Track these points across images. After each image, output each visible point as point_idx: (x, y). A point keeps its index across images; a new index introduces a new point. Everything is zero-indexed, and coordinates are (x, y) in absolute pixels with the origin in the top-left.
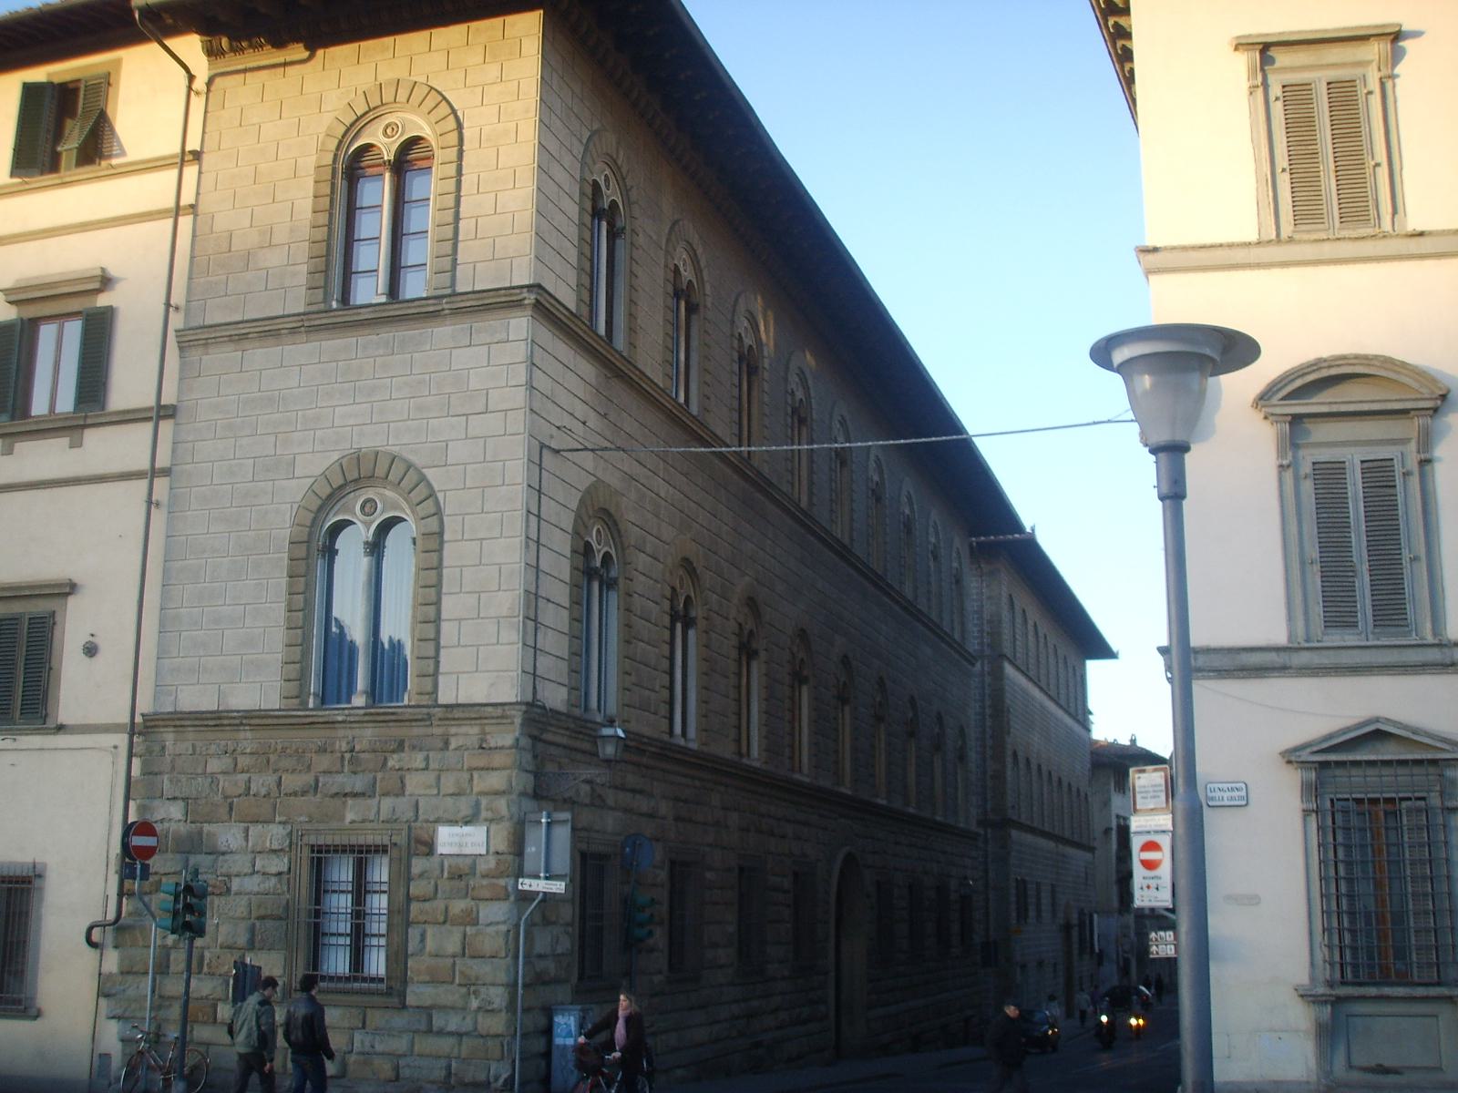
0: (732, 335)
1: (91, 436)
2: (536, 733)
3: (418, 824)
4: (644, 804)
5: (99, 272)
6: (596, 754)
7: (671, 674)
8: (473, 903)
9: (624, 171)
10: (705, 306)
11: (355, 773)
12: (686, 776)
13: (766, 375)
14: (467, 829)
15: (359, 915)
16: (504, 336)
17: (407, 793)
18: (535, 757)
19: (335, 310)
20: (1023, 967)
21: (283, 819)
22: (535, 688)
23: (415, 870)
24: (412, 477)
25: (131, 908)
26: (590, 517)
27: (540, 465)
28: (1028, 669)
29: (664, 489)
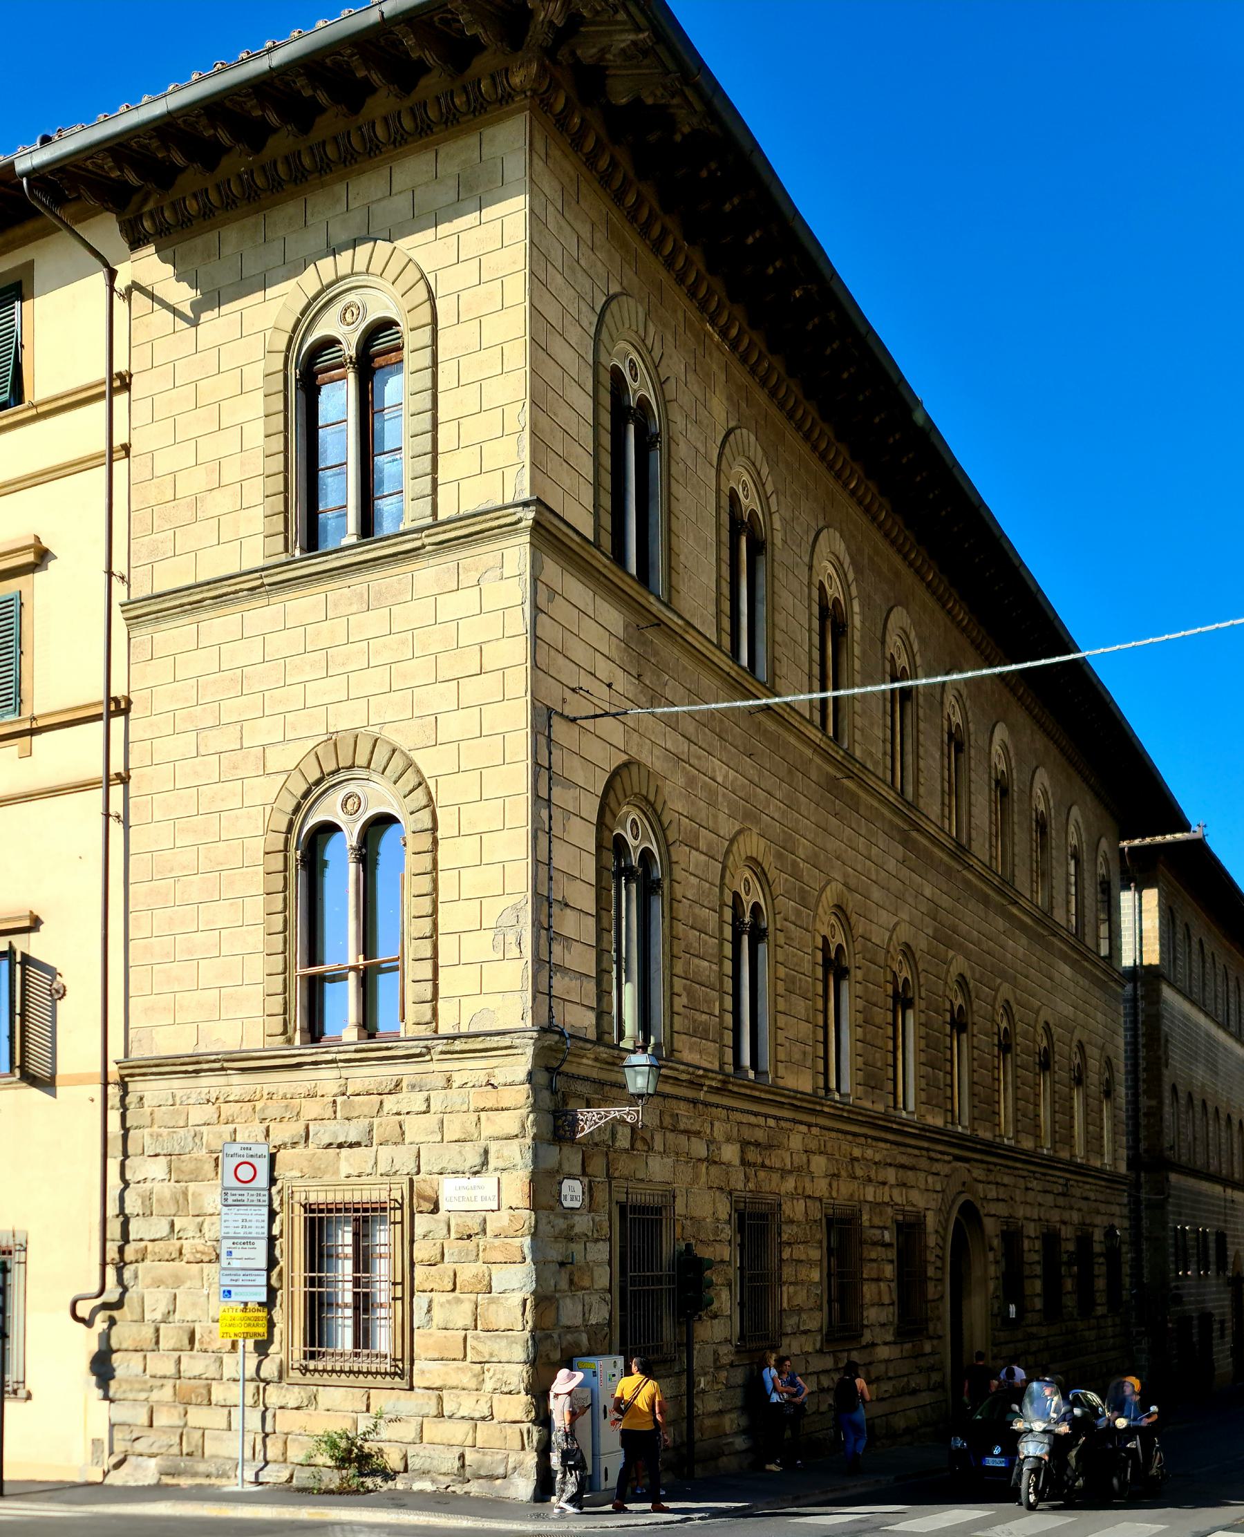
3: (421, 1176)
5: (32, 541)
6: (623, 1086)
12: (756, 1114)
14: (476, 1181)
17: (407, 1141)
28: (1191, 991)
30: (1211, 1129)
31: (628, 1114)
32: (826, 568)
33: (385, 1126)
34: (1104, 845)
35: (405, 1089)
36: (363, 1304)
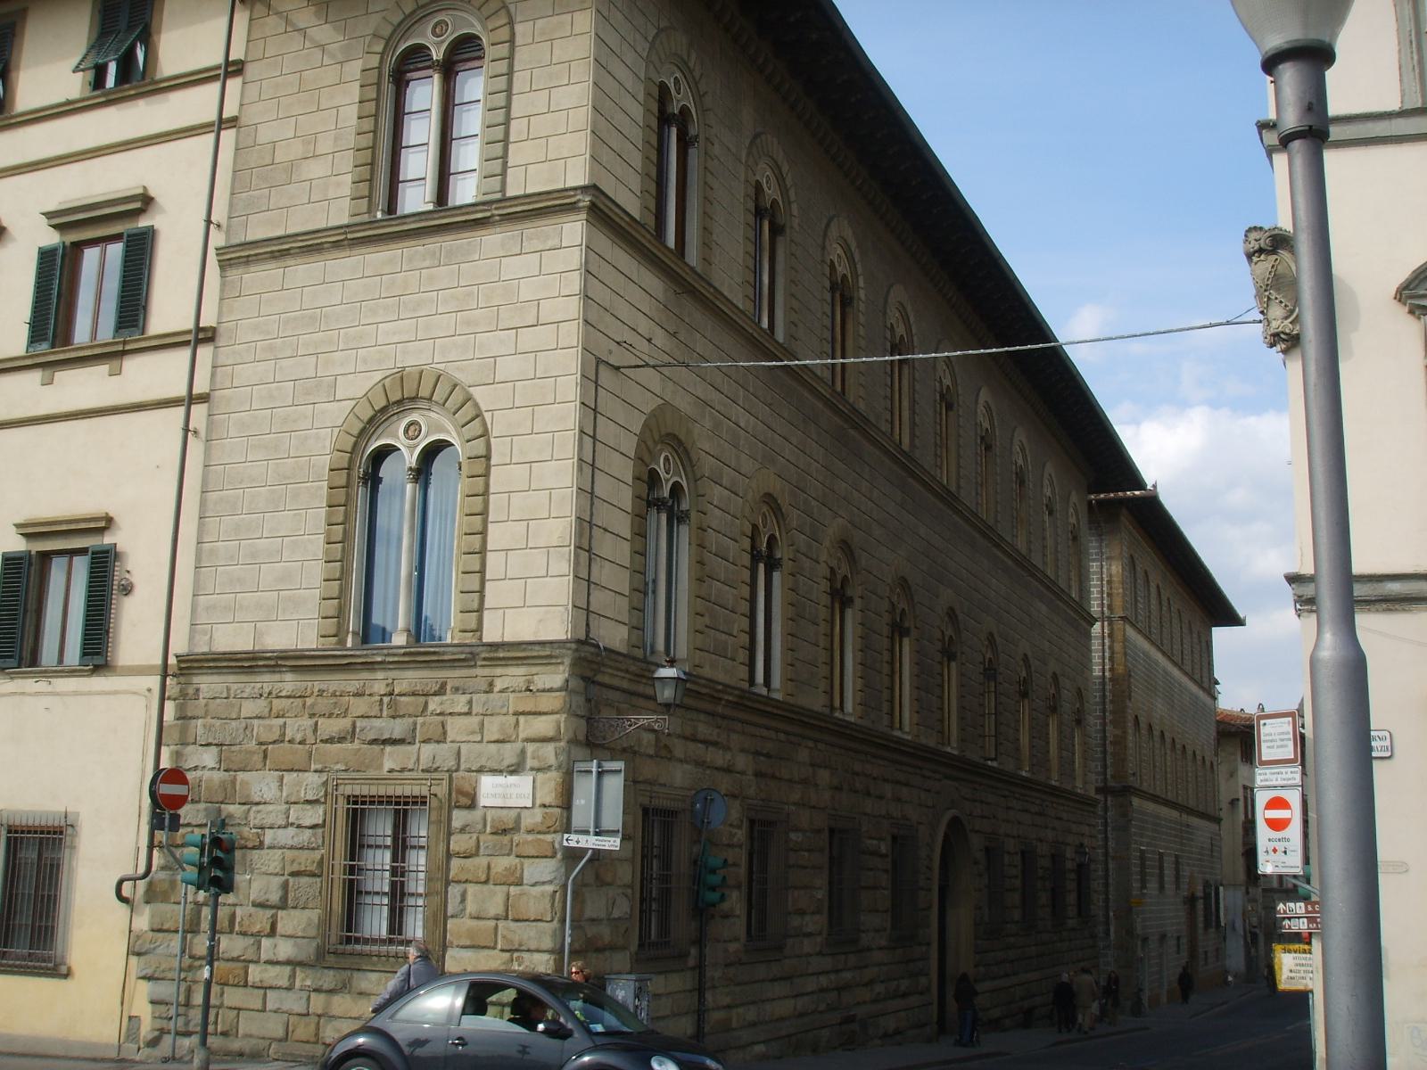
0: (823, 261)
1: (131, 364)
2: (589, 674)
3: (461, 774)
4: (719, 757)
5: (140, 191)
6: (654, 698)
7: (752, 617)
8: (518, 860)
9: (697, 74)
10: (792, 227)
11: (393, 717)
12: (768, 728)
13: (862, 307)
14: (512, 779)
15: (398, 872)
16: (556, 242)
17: (449, 739)
18: (588, 700)
19: (381, 220)
20: (1145, 940)
21: (319, 767)
22: (588, 625)
23: (456, 824)
24: (457, 397)
25: (162, 862)
26: (656, 443)
27: (596, 382)
28: (1162, 643)
29: (737, 413)
30: (1168, 758)
31: (656, 721)
32: (836, 252)
33: (425, 724)
34: (1074, 498)
35: (448, 691)
36: (398, 895)
